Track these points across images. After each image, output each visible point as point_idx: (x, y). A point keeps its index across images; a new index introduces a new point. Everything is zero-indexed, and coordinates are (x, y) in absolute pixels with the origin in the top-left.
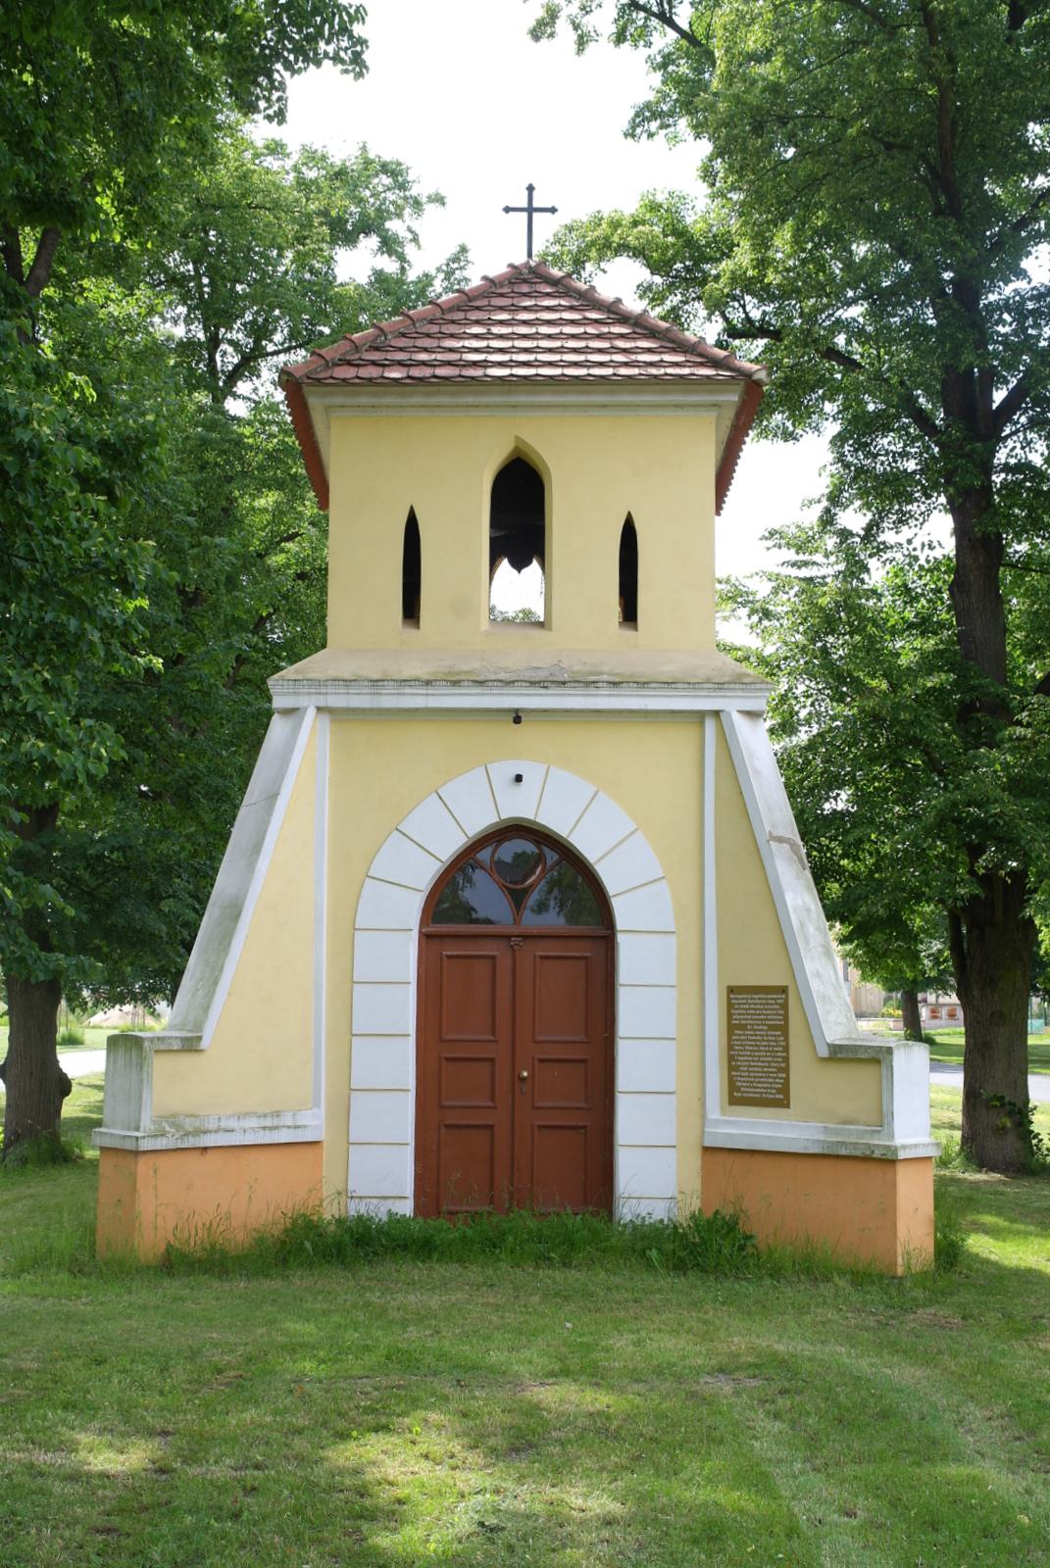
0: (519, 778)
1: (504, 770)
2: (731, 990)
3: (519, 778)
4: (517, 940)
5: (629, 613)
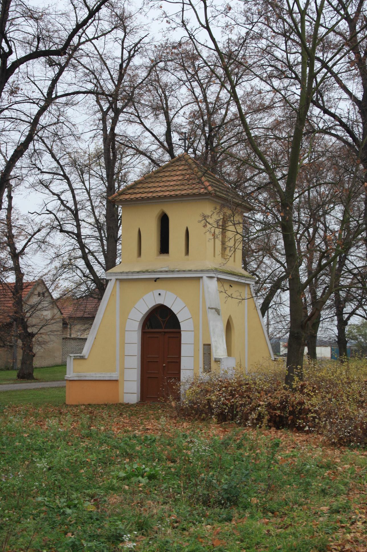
0: (160, 294)
2: (204, 345)
3: (160, 294)
4: (161, 326)
5: (187, 252)
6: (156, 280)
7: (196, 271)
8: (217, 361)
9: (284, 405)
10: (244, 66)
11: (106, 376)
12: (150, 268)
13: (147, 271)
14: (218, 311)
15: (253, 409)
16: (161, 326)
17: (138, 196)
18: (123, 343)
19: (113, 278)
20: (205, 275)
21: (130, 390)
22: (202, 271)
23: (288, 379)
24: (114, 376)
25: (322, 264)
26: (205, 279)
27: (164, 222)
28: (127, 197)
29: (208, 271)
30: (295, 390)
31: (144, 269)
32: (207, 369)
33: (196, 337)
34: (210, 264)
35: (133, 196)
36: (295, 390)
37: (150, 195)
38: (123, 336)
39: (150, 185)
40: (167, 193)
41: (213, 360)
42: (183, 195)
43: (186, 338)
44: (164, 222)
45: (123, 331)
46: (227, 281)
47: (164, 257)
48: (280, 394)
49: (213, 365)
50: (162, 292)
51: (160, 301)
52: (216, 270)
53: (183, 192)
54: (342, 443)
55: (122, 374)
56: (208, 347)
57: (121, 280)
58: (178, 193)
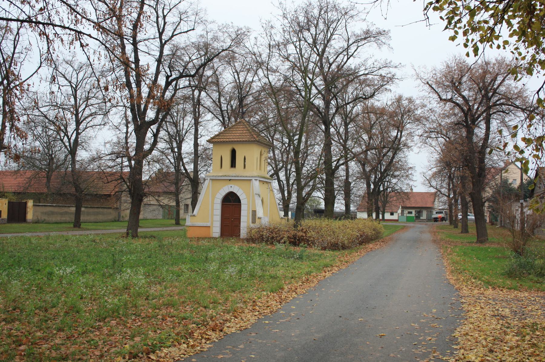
1: (230, 186)
4: (231, 202)
6: (230, 180)
7: (249, 177)
8: (260, 218)
9: (295, 237)
10: (483, 281)
11: (205, 224)
12: (227, 174)
13: (225, 176)
14: (259, 196)
15: (282, 239)
16: (231, 202)
17: (222, 140)
18: (213, 209)
19: (209, 178)
20: (253, 179)
21: (216, 231)
22: (252, 177)
23: (295, 226)
24: (208, 224)
25: (192, 177)
26: (253, 180)
27: (233, 153)
28: (216, 140)
29: (255, 177)
30: (299, 231)
31: (224, 175)
32: (254, 221)
33: (248, 207)
34: (255, 174)
35: (219, 140)
36: (299, 231)
37: (227, 140)
38: (213, 206)
39: (227, 135)
40: (236, 140)
41: (257, 218)
42: (243, 141)
43: (244, 207)
44: (233, 153)
45: (213, 203)
46: (264, 181)
47: (233, 169)
48: (293, 233)
49: (257, 219)
50: (233, 186)
51: (231, 190)
52: (259, 177)
53: (244, 139)
54: (324, 249)
55: (212, 223)
56: (254, 213)
57: (212, 180)
58: (241, 139)
